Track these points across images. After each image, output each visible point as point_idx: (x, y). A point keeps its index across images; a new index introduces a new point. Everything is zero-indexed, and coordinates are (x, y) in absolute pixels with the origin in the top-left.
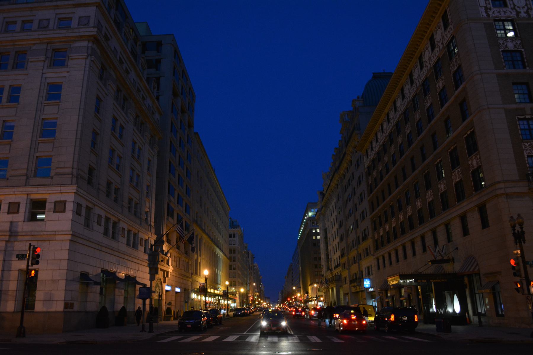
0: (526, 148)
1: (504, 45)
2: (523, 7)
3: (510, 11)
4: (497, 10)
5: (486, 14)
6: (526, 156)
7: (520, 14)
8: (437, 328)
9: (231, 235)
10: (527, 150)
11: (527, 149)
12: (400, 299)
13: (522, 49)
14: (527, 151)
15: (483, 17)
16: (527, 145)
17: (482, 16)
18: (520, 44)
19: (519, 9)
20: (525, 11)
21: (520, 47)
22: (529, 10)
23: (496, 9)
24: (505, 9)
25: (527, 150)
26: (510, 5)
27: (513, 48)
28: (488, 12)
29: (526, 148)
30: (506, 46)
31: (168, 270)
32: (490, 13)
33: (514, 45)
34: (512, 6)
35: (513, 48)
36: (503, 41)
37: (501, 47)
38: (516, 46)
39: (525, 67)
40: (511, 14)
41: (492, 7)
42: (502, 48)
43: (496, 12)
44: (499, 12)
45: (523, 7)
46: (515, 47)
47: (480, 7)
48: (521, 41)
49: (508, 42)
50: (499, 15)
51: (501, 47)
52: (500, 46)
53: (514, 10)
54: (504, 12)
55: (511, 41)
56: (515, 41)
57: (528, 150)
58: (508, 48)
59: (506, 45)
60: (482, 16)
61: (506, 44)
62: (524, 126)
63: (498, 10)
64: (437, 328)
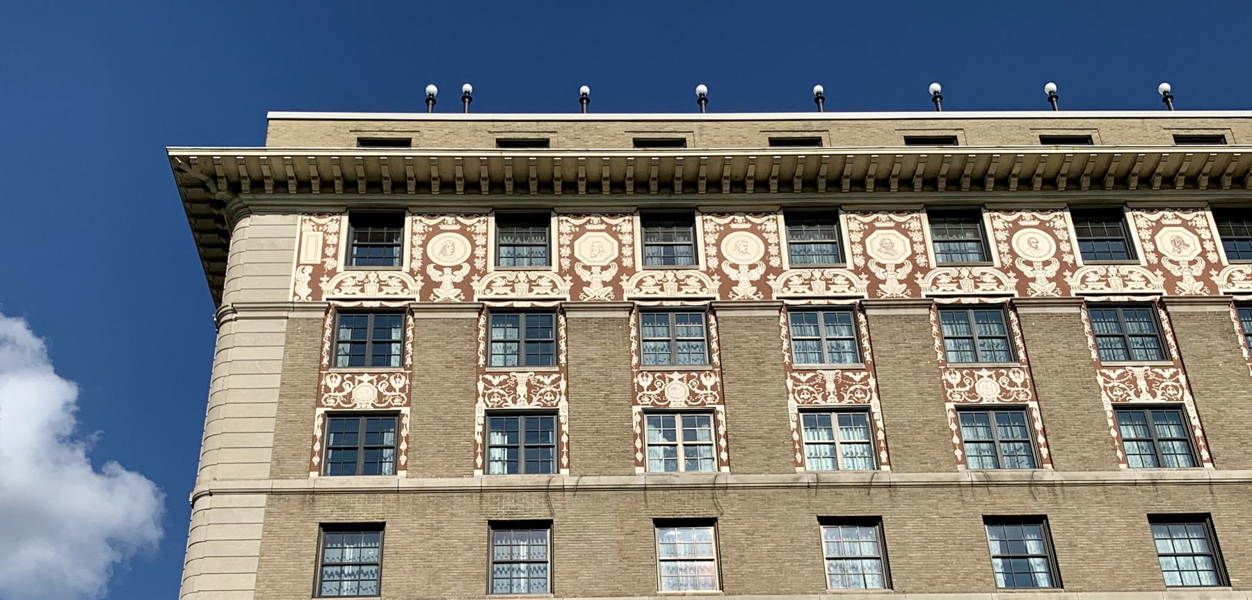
0: (490, 391)
1: (341, 394)
2: (1046, 263)
3: (403, 282)
4: (800, 276)
5: (310, 291)
7: (1031, 284)
13: (718, 404)
15: (297, 298)
16: (496, 381)
17: (295, 294)
18: (714, 388)
19: (587, 272)
20: (1199, 273)
21: (710, 399)
22: (1213, 272)
23: (1095, 268)
24: (1124, 269)
26: (412, 258)
27: (683, 404)
28: (321, 282)
30: (973, 390)
32: (1220, 280)
34: (566, 264)
35: (373, 405)
36: (343, 381)
37: (640, 398)
38: (697, 394)
39: (1035, 462)
40: (998, 286)
41: (786, 266)
42: (646, 400)
43: (1238, 276)
44: (957, 280)
45: (1046, 263)
47: (298, 265)
49: (671, 380)
50: (1104, 287)
51: (640, 398)
52: (640, 394)
53: (1159, 273)
54: (530, 281)
56: (388, 381)
58: (978, 400)
59: (663, 392)
60: (295, 294)
61: (348, 390)
63: (1101, 270)
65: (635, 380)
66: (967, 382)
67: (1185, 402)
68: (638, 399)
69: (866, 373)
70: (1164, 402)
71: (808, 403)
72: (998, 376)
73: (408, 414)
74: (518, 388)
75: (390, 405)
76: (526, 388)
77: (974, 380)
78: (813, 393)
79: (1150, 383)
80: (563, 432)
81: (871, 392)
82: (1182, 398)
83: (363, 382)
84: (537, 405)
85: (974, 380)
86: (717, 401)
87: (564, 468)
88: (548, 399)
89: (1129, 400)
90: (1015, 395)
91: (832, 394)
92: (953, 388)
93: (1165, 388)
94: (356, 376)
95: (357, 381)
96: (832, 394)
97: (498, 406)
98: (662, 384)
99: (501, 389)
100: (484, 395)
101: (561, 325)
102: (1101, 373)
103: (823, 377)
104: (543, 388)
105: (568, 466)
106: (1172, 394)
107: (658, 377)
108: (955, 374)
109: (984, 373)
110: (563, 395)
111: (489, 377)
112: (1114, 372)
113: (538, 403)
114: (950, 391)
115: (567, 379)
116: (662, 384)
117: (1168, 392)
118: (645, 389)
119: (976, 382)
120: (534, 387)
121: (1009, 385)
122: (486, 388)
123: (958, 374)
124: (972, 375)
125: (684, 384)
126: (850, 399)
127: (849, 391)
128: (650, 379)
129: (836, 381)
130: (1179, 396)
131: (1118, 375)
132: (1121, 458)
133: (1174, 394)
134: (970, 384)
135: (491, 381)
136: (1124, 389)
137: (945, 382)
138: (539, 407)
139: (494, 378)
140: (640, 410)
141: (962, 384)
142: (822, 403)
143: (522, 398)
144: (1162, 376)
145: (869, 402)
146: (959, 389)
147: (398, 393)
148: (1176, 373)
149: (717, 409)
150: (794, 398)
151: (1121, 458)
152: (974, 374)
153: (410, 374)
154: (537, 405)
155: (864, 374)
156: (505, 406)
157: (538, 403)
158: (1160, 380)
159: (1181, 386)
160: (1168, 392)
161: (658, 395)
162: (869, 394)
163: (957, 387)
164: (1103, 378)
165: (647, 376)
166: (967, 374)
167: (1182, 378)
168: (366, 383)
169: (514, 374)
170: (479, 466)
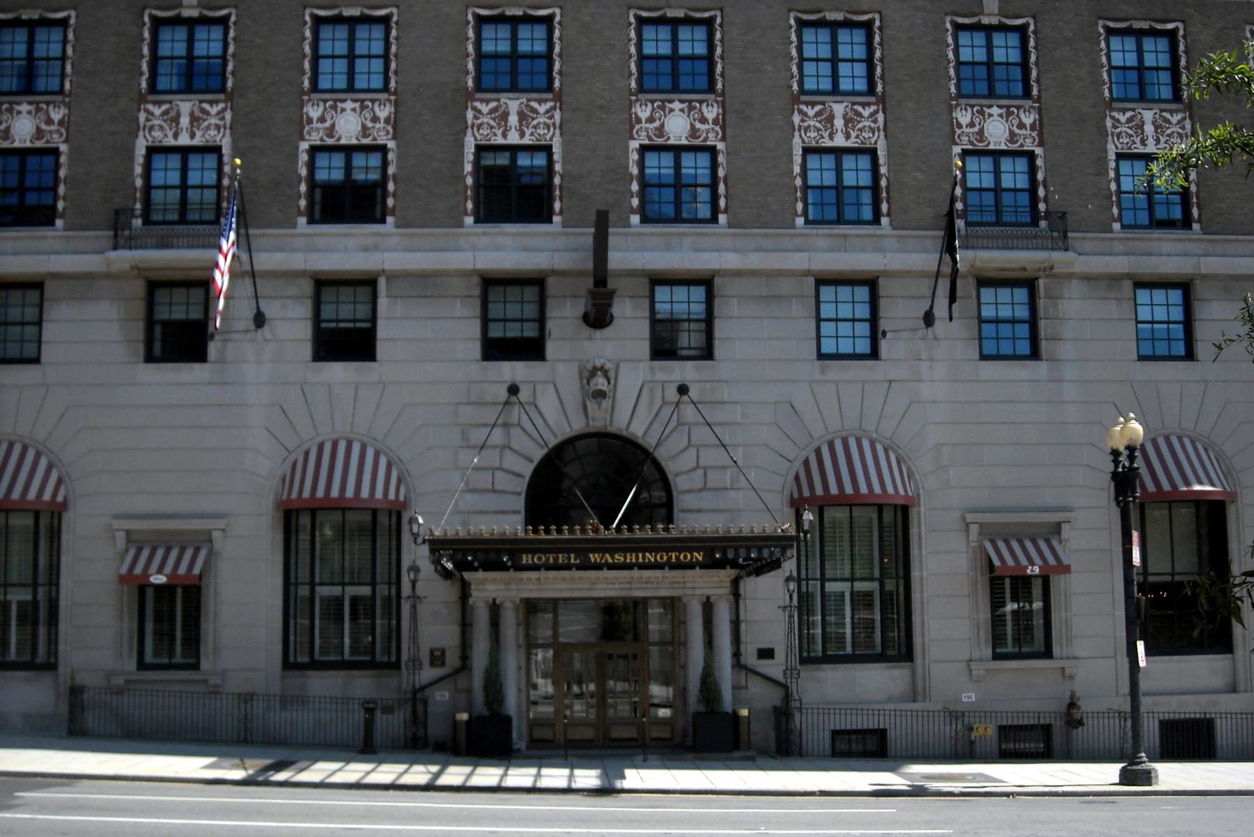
0: (1118, 130)
6: (1112, 156)
8: (728, 567)
9: (1150, 785)
10: (807, 129)
11: (809, 126)
12: (1007, 577)
14: (1118, 140)
16: (1123, 118)
25: (807, 129)
29: (1118, 130)
30: (981, 132)
31: (1037, 610)
33: (1011, 132)
38: (698, 130)
46: (1009, 142)
48: (1037, 117)
49: (990, 115)
52: (637, 127)
55: (1001, 116)
56: (1018, 116)
57: (812, 128)
62: (1016, 216)
64: (728, 567)
65: (633, 110)
66: (977, 121)
67: (553, 143)
68: (956, 137)
69: (1183, 115)
70: (531, 142)
71: (486, 140)
72: (1009, 114)
73: (1042, 155)
74: (1145, 127)
75: (1022, 145)
76: (843, 121)
77: (984, 119)
78: (1131, 136)
79: (194, 119)
80: (882, 175)
81: (879, 131)
82: (876, 143)
83: (993, 115)
84: (855, 143)
85: (984, 119)
86: (1036, 143)
87: (884, 216)
88: (542, 133)
89: (1135, 148)
90: (1021, 141)
91: (513, 128)
92: (962, 128)
93: (861, 130)
94: (985, 109)
95: (339, 109)
96: (513, 128)
97: (486, 140)
98: (661, 115)
99: (1128, 127)
100: (800, 127)
101: (69, 42)
102: (1110, 115)
103: (1142, 117)
104: (861, 121)
105: (889, 214)
106: (866, 136)
107: (657, 107)
108: (713, 106)
109: (995, 111)
110: (558, 128)
111: (804, 107)
112: (1124, 114)
113: (855, 140)
114: (958, 131)
115: (1191, 118)
116: (661, 115)
117: (863, 134)
118: (964, 127)
119: (665, 116)
120: (1160, 126)
121: (1018, 127)
122: (476, 117)
123: (650, 105)
124: (981, 112)
125: (356, 115)
126: (1165, 143)
127: (857, 128)
128: (321, 109)
129: (844, 117)
130: (873, 141)
131: (1128, 119)
132: (1116, 216)
133: (545, 134)
134: (979, 124)
135: (1169, 120)
136: (819, 130)
137: (955, 121)
138: (857, 145)
139: (1172, 116)
140: (638, 146)
141: (972, 125)
142: (1141, 150)
143: (184, 132)
144: (1168, 121)
145: (876, 143)
146: (969, 130)
147: (711, 126)
148: (876, 112)
149: (718, 148)
150: (801, 136)
151: (1116, 216)
152: (985, 112)
153: (70, 102)
154: (855, 143)
155: (873, 108)
156: (1135, 148)
157: (855, 140)
158: (1167, 125)
159: (878, 128)
160: (1172, 140)
161: (656, 129)
162: (552, 129)
163: (317, 123)
164: (473, 112)
165: (966, 110)
166: (658, 107)
167: (880, 117)
168: (996, 117)
169: (1141, 111)
170: (469, 212)
